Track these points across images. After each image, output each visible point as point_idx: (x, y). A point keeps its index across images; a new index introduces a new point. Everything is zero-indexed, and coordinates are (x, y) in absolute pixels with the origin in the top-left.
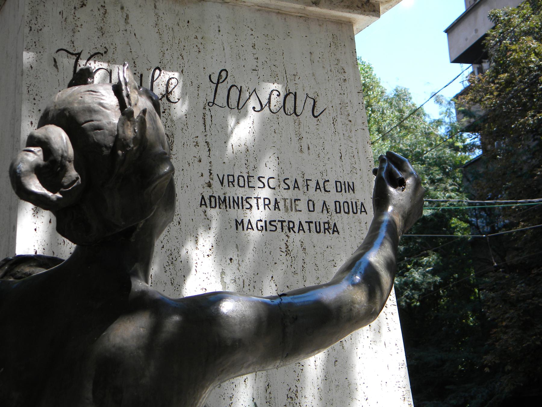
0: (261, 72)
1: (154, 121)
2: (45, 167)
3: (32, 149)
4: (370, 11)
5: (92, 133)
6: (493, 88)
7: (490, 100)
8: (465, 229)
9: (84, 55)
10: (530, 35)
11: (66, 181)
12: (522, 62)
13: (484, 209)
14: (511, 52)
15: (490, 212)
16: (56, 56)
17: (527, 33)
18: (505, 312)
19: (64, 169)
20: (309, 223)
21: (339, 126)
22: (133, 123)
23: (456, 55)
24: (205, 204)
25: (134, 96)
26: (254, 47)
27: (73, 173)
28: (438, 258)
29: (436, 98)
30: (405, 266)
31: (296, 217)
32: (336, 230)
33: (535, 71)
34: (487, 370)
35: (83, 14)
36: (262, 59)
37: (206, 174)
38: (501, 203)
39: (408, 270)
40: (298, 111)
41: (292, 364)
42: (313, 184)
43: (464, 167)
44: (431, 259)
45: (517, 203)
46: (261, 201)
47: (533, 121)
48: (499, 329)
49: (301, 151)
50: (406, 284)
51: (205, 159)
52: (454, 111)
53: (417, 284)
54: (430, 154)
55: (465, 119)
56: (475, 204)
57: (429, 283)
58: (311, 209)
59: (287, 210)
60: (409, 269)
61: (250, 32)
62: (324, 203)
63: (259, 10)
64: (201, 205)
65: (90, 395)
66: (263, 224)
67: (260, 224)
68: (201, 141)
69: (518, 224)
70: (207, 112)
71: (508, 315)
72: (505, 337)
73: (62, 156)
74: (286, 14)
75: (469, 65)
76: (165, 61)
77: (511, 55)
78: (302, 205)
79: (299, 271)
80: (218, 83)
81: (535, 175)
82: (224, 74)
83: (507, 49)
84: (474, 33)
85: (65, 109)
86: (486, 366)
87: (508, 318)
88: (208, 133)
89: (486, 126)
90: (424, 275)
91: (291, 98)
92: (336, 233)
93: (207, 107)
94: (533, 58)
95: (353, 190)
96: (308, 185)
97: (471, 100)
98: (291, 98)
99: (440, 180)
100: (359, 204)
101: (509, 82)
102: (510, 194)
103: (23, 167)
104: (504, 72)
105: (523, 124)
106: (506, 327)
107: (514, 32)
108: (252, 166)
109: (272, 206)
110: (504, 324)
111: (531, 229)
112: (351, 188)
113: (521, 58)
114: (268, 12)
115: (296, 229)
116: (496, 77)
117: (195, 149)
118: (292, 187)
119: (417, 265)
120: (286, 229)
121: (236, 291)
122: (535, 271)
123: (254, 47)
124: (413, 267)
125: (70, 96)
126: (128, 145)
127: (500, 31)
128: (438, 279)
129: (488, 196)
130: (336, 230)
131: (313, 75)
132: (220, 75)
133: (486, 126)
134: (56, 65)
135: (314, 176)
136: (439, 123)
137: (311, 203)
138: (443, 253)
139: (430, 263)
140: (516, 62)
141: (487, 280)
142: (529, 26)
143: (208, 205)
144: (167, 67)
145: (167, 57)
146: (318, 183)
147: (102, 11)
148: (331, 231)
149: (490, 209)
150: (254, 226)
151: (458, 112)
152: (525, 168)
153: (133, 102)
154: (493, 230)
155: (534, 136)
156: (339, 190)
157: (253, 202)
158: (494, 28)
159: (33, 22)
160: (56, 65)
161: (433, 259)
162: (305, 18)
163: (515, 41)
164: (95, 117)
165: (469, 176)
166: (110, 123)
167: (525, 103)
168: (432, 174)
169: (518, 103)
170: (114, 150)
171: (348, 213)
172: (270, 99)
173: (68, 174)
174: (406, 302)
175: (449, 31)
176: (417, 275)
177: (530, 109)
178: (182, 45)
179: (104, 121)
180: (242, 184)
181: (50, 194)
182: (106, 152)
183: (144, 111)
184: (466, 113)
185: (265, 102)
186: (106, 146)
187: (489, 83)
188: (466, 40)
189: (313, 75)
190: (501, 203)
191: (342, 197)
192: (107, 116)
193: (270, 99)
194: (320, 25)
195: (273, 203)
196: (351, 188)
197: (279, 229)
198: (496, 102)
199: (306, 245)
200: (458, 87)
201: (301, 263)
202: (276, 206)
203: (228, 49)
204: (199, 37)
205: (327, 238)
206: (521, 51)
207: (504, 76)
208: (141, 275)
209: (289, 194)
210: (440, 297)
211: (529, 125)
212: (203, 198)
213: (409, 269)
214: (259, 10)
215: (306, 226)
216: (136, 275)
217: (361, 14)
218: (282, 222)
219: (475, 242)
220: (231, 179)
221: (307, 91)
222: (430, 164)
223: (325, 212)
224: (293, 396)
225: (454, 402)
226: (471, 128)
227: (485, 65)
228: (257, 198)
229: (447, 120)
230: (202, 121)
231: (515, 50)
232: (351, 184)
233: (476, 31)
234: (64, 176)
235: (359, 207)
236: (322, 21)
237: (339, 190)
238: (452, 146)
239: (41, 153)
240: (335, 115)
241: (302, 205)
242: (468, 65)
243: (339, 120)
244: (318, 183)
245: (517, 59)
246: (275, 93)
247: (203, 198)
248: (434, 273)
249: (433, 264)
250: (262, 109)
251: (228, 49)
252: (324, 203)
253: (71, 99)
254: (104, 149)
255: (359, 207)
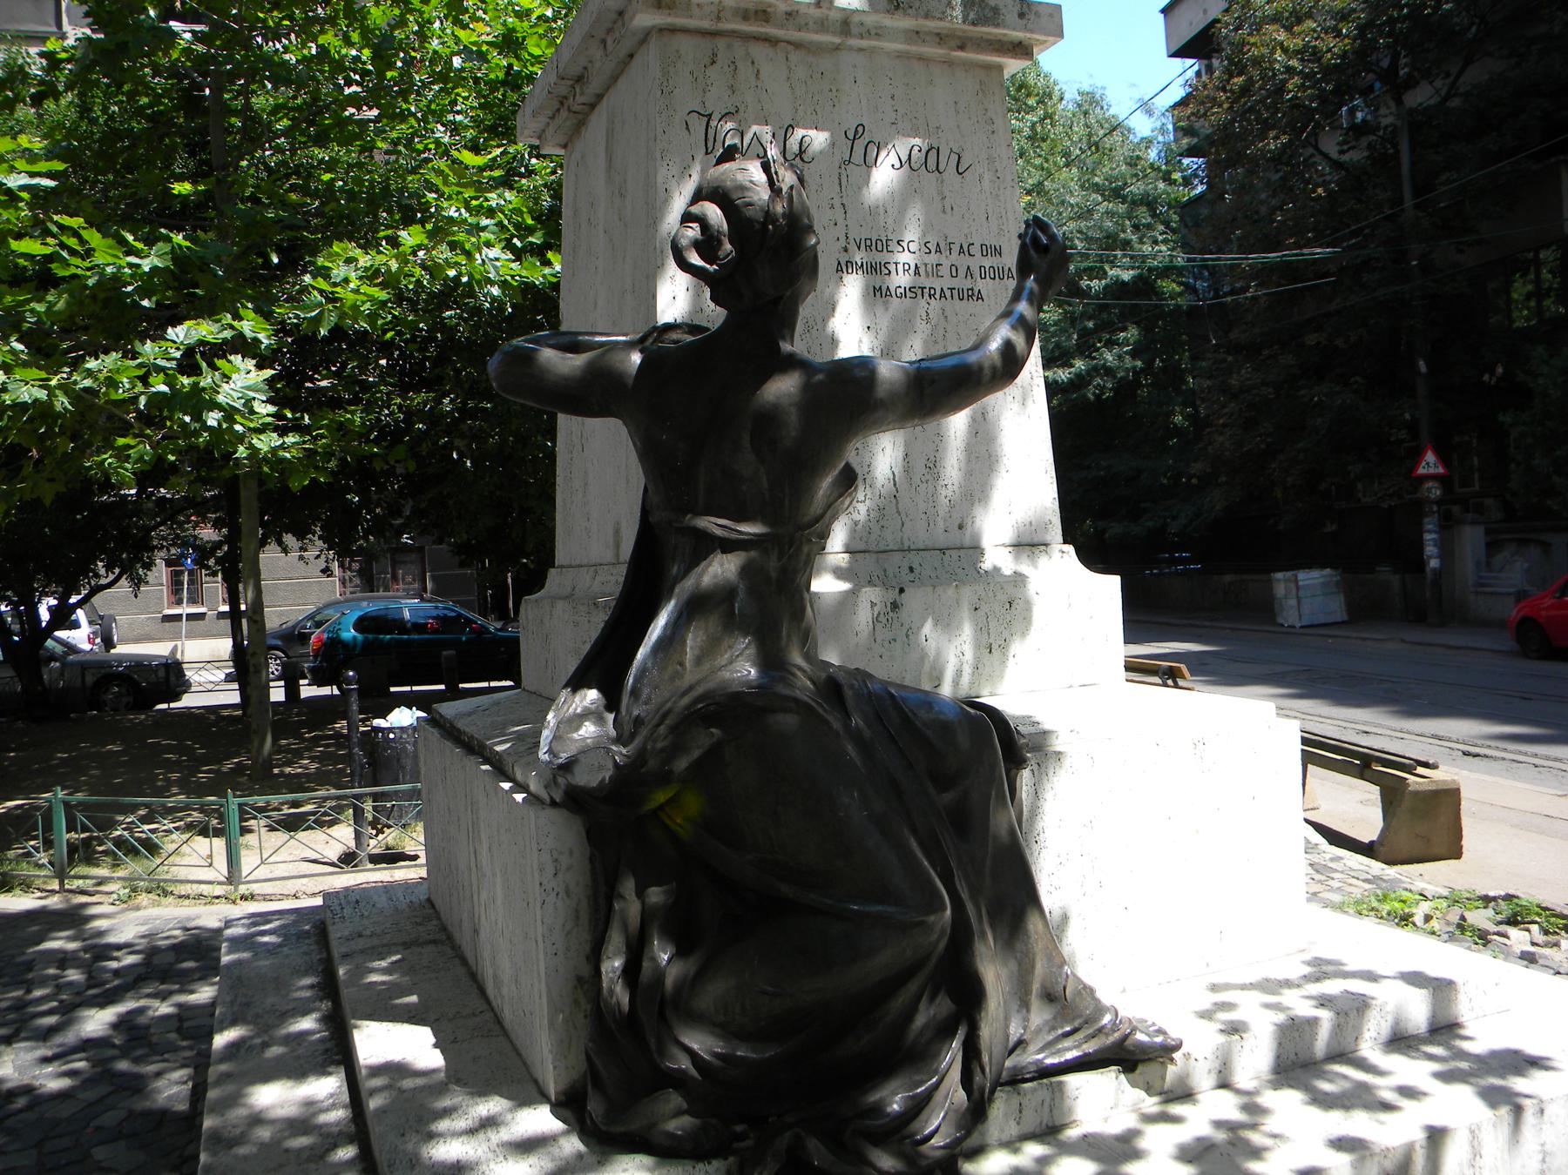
0: (901, 126)
1: (800, 195)
2: (702, 241)
3: (690, 225)
4: (1022, 54)
5: (744, 209)
6: (1223, 98)
7: (1219, 115)
8: (1180, 294)
9: (716, 116)
10: (1277, 23)
11: (721, 254)
12: (1264, 61)
13: (1206, 267)
14: (1248, 47)
15: (1213, 271)
16: (687, 118)
17: (1275, 19)
18: (1224, 407)
19: (720, 243)
20: (951, 289)
21: (986, 183)
22: (782, 199)
23: (1175, 47)
24: (842, 270)
25: (781, 172)
26: (893, 97)
27: (728, 247)
28: (1139, 334)
29: (1146, 107)
30: (1094, 345)
31: (937, 284)
32: (980, 297)
33: (1282, 74)
34: (1194, 481)
35: (713, 72)
36: (901, 111)
37: (843, 238)
38: (1227, 258)
39: (1098, 350)
40: (941, 168)
41: (931, 426)
42: (956, 248)
43: (1182, 207)
44: (1132, 333)
45: (1248, 259)
46: (900, 267)
47: (1276, 146)
48: (1214, 429)
49: (944, 212)
50: (1095, 369)
51: (840, 221)
52: (1170, 127)
53: (1110, 368)
54: (1136, 188)
55: (1185, 141)
56: (1194, 260)
57: (1127, 370)
58: (954, 274)
59: (928, 275)
60: (1099, 348)
61: (889, 81)
62: (968, 268)
63: (898, 57)
64: (837, 271)
65: (748, 445)
66: (902, 290)
67: (899, 291)
68: (837, 203)
69: (1245, 289)
70: (843, 171)
71: (1226, 410)
72: (1221, 439)
73: (718, 231)
74: (928, 60)
75: (1194, 61)
76: (798, 118)
77: (1249, 51)
78: (944, 271)
79: (940, 339)
80: (854, 139)
81: (1275, 221)
82: (860, 129)
83: (1244, 44)
84: (1201, 14)
85: (718, 187)
86: (1194, 476)
87: (1226, 414)
88: (844, 194)
89: (1213, 150)
90: (1120, 357)
91: (933, 153)
92: (980, 301)
93: (843, 166)
94: (1278, 56)
95: (1000, 254)
96: (950, 249)
97: (1193, 114)
98: (933, 153)
99: (1149, 227)
100: (1006, 269)
101: (1245, 90)
102: (1240, 246)
103: (684, 242)
104: (1239, 75)
105: (1262, 150)
106: (1225, 425)
107: (1256, 17)
108: (891, 229)
109: (912, 271)
110: (1221, 421)
111: (1264, 294)
112: (998, 251)
113: (1263, 55)
114: (909, 58)
115: (937, 296)
116: (1228, 82)
117: (831, 212)
118: (933, 251)
119: (1110, 344)
120: (926, 296)
121: (877, 352)
122: (1266, 352)
123: (893, 97)
124: (1105, 346)
125: (722, 174)
126: (778, 220)
127: (1236, 15)
128: (1139, 363)
129: (452, 401)
130: (980, 297)
131: (958, 127)
132: (856, 131)
133: (1213, 150)
134: (688, 129)
135: (958, 239)
136: (1148, 142)
137: (954, 268)
138: (1147, 329)
139: (1128, 340)
140: (1256, 62)
141: (1204, 364)
142: (1276, 8)
143: (845, 270)
144: (801, 124)
145: (800, 113)
146: (961, 247)
147: (733, 67)
148: (975, 298)
149: (1214, 266)
150: (893, 293)
151: (1176, 129)
152: (1263, 210)
153: (780, 179)
154: (1217, 296)
155: (1275, 167)
156: (985, 253)
157: (892, 268)
158: (1227, 11)
159: (665, 84)
160: (688, 129)
161: (1132, 335)
162: (950, 63)
163: (1256, 30)
164: (746, 194)
165: (1188, 220)
166: (760, 199)
167: (1267, 119)
168: (1136, 217)
169: (1256, 119)
170: (764, 224)
171: (994, 279)
172: (910, 155)
173: (723, 248)
174: (1094, 393)
175: (1165, 11)
176: (1109, 357)
177: (1273, 128)
178: (815, 98)
179: (756, 198)
180: (880, 248)
181: (708, 266)
182: (757, 226)
183: (791, 188)
184: (1188, 131)
185: (904, 159)
186: (757, 221)
187: (1218, 89)
188: (1191, 24)
189: (958, 127)
190: (1227, 258)
191: (987, 262)
192: (758, 193)
193: (910, 155)
194: (966, 71)
195: (913, 268)
196: (998, 251)
197: (919, 296)
198: (1226, 118)
199: (948, 313)
200: (1177, 93)
201: (942, 332)
202: (917, 272)
203: (864, 102)
204: (834, 90)
205: (972, 306)
206: (1263, 45)
207: (1239, 80)
208: (788, 338)
209: (933, 259)
210: (1140, 386)
211: (1269, 151)
212: (839, 263)
213: (1099, 348)
214: (898, 57)
215: (948, 293)
216: (784, 338)
217: (1012, 58)
218: (923, 288)
219: (1193, 312)
220: (868, 243)
221: (951, 145)
222: (1134, 203)
223: (969, 277)
224: (932, 466)
225: (1150, 524)
226: (1191, 152)
227: (1216, 62)
228: (896, 264)
229: (1160, 138)
230: (837, 182)
231: (1254, 44)
232: (998, 248)
233: (1205, 11)
234: (719, 249)
235: (1006, 273)
236: (969, 66)
237: (985, 253)
238: (1167, 178)
239: (698, 229)
240: (982, 170)
241: (944, 271)
242: (1192, 61)
243: (986, 177)
244: (961, 247)
245: (1258, 56)
246: (916, 148)
247: (839, 263)
248: (1134, 354)
249: (1131, 341)
250: (901, 166)
251: (864, 102)
252: (968, 268)
253: (723, 177)
254: (756, 224)
255: (1006, 273)
